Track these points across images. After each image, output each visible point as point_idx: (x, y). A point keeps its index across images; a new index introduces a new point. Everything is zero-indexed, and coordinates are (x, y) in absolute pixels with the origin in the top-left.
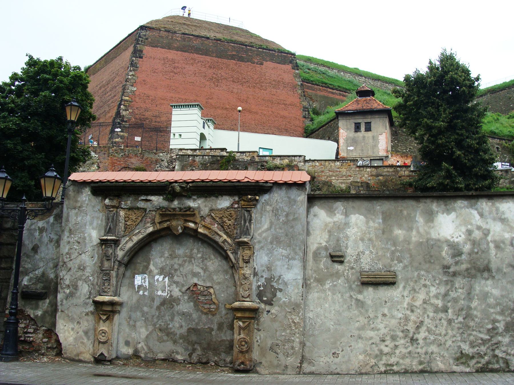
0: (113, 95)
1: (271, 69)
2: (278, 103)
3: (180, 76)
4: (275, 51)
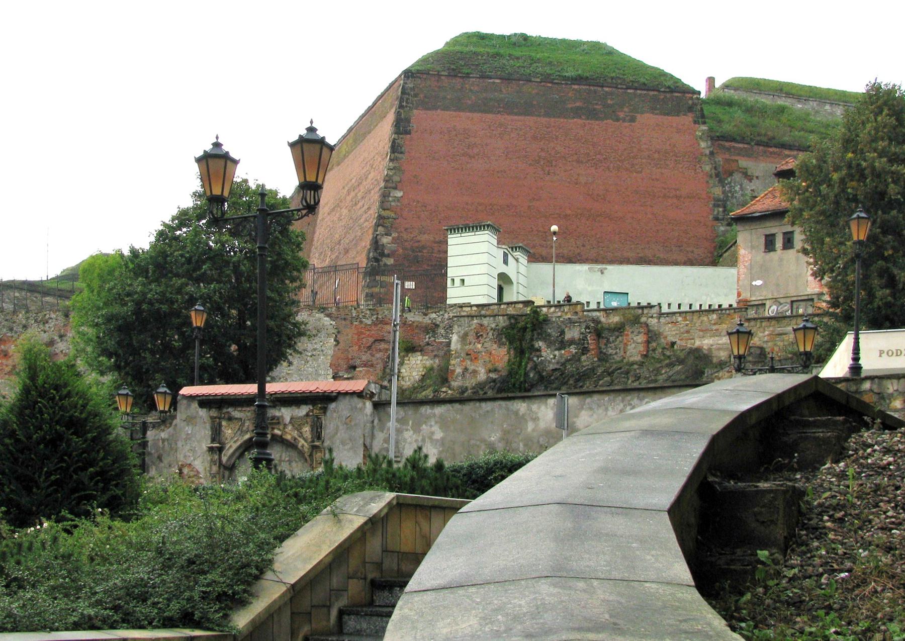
0: (366, 207)
1: (652, 128)
2: (665, 196)
4: (659, 91)
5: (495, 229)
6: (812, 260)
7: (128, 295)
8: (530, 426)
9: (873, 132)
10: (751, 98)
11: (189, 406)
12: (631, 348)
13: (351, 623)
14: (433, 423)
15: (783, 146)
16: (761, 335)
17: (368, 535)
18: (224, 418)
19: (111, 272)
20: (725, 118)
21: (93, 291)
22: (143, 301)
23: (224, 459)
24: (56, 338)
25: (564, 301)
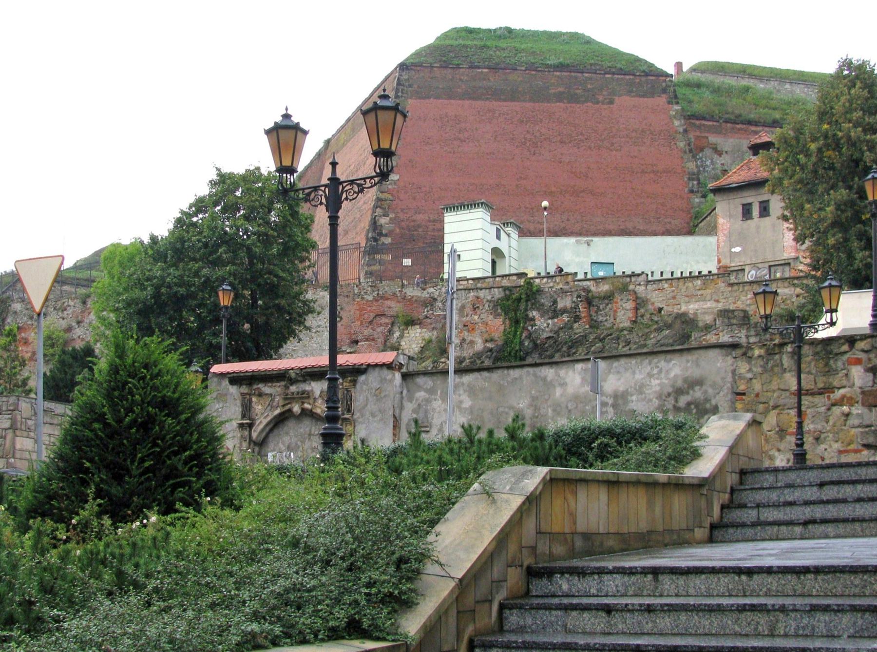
1: (629, 110)
3: (470, 144)
4: (634, 75)
5: (487, 206)
6: (792, 226)
7: (148, 279)
8: (558, 392)
9: (847, 104)
10: (718, 80)
11: (220, 384)
12: (620, 314)
13: (513, 618)
14: (461, 392)
15: (750, 123)
16: (744, 298)
17: (524, 515)
18: (254, 394)
19: (131, 259)
20: (696, 98)
21: (113, 278)
22: (162, 285)
23: (254, 435)
24: (74, 324)
25: (555, 272)
